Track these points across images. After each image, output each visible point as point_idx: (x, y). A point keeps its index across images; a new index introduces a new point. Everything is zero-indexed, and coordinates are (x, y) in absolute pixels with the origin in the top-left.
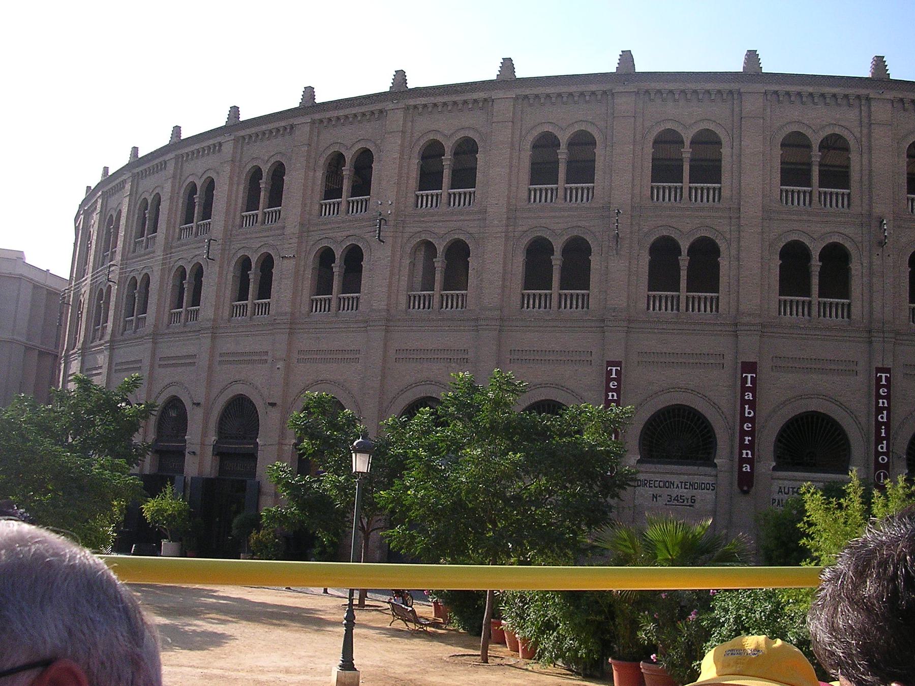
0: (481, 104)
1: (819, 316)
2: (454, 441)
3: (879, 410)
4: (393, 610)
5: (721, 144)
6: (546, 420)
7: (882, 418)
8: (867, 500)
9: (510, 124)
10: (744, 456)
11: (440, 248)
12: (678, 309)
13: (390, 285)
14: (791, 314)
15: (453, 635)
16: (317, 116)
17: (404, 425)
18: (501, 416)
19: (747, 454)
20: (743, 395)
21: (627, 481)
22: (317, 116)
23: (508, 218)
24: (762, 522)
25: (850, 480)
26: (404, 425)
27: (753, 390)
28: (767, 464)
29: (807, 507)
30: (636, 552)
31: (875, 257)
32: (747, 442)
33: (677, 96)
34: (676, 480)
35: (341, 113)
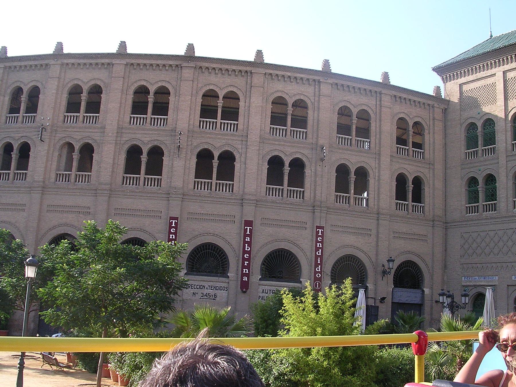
0: (106, 66)
1: (287, 197)
2: (84, 260)
3: (317, 249)
4: (43, 358)
5: (239, 99)
6: (136, 249)
7: (319, 253)
8: (315, 297)
9: (122, 79)
10: (244, 272)
11: (77, 147)
12: (211, 190)
13: (46, 167)
14: (272, 195)
15: (79, 373)
16: (8, 64)
17: (52, 249)
18: (112, 247)
19: (246, 271)
20: (245, 239)
21: (183, 285)
22: (8, 64)
23: (117, 132)
24: (254, 309)
25: (306, 287)
26: (52, 249)
27: (250, 236)
28: (256, 276)
29: (284, 301)
30: (188, 325)
31: (318, 167)
32: (246, 264)
33: (217, 71)
34: (206, 284)
35: (23, 64)
